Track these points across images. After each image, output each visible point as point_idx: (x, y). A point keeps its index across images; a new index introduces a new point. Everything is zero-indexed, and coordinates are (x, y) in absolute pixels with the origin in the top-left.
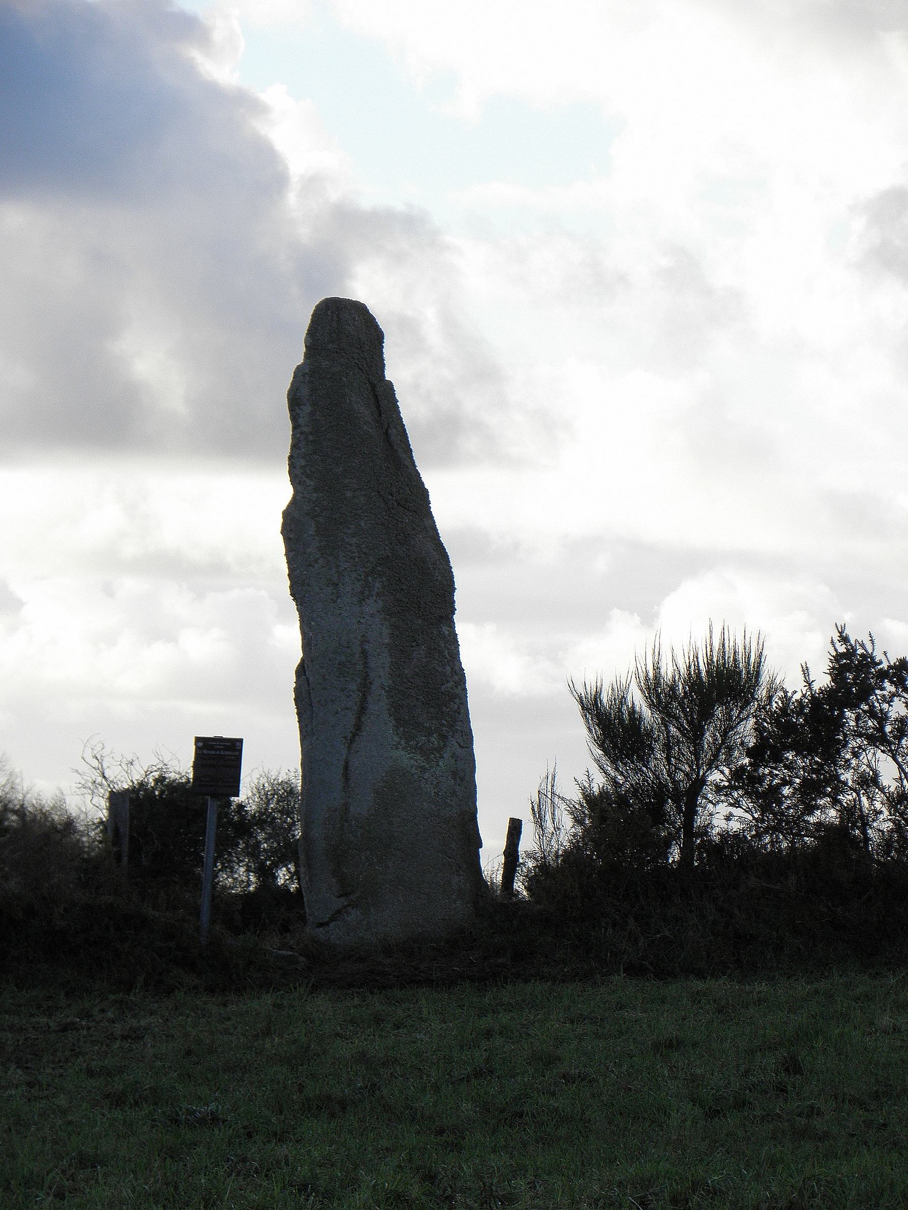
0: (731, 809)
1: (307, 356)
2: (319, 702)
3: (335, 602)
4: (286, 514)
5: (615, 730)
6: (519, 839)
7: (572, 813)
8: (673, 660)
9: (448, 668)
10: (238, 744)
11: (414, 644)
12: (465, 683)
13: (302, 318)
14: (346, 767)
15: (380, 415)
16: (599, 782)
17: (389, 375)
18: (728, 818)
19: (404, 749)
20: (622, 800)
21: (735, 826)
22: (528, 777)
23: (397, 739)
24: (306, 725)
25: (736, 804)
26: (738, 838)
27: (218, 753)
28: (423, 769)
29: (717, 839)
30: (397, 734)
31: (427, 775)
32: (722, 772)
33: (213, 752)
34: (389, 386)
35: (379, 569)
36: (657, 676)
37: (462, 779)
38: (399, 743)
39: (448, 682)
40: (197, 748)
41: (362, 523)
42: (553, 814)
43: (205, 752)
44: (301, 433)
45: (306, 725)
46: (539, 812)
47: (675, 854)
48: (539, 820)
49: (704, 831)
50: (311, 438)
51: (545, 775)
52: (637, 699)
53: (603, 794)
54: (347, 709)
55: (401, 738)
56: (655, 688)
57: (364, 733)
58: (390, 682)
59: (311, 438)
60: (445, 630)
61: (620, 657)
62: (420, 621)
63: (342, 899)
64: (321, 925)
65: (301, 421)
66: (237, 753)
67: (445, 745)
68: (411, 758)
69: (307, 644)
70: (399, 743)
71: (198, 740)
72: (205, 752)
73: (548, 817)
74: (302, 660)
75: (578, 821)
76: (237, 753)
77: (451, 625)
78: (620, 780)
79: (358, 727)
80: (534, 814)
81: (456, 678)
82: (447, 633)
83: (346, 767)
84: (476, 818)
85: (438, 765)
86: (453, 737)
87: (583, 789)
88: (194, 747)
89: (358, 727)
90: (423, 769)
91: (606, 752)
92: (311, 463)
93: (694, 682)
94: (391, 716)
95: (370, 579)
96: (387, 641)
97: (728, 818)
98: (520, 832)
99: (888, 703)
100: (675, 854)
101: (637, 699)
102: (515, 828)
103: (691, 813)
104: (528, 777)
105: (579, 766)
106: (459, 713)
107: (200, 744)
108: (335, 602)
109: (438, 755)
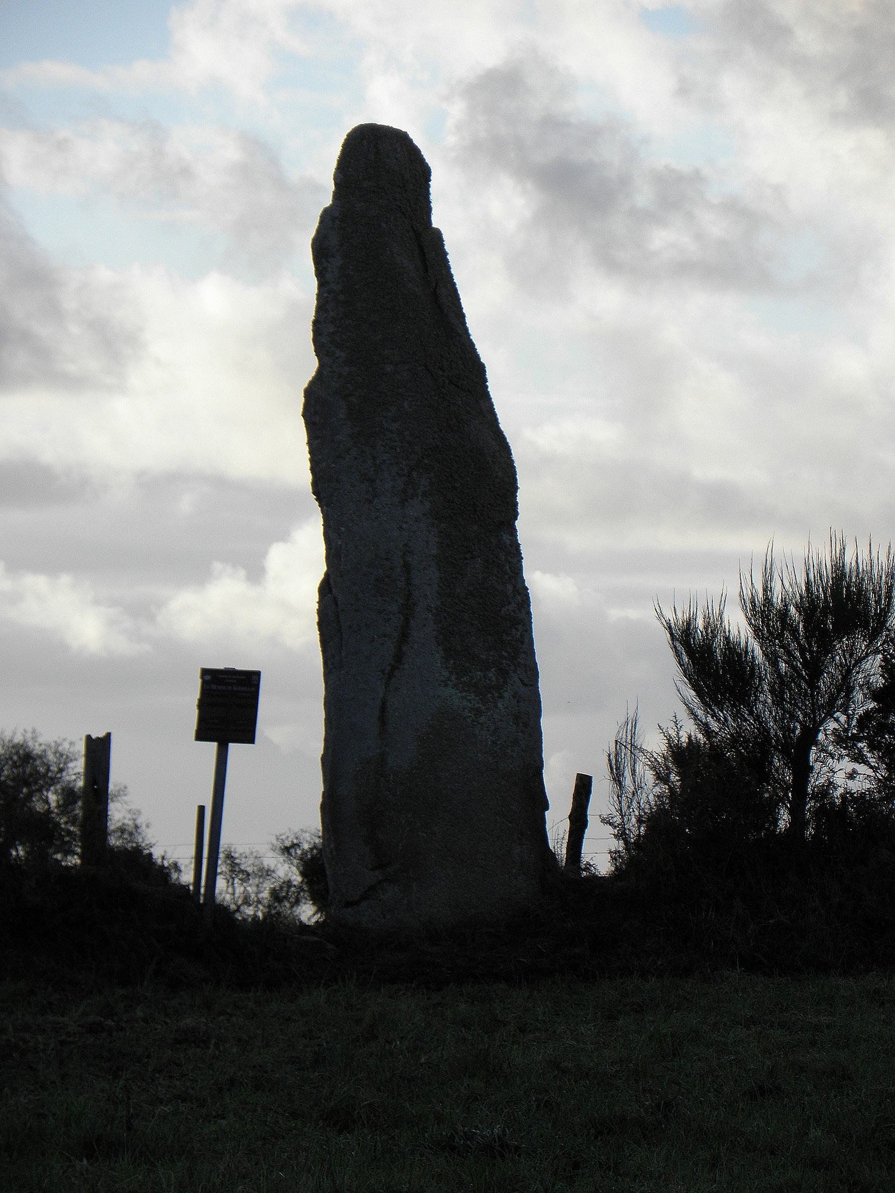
0: (857, 766)
1: (337, 195)
2: (350, 627)
3: (370, 502)
4: (309, 393)
5: (707, 662)
6: (588, 801)
7: (653, 768)
8: (857, 562)
9: (510, 587)
10: (254, 677)
11: (468, 556)
12: (529, 606)
13: (315, 175)
14: (383, 709)
15: (426, 270)
16: (689, 730)
17: (437, 221)
18: (852, 776)
19: (455, 686)
20: (715, 753)
21: (858, 786)
22: (604, 723)
23: (446, 673)
24: (333, 656)
25: (859, 758)
26: (860, 800)
27: (230, 688)
28: (478, 712)
29: (838, 802)
30: (447, 668)
31: (482, 719)
32: (837, 720)
33: (224, 688)
34: (437, 236)
35: (426, 461)
36: (768, 601)
37: (526, 725)
38: (449, 679)
39: (510, 603)
40: (204, 683)
41: (406, 405)
42: (634, 772)
43: (214, 687)
44: (329, 292)
45: (333, 656)
46: (618, 769)
47: (784, 819)
48: (617, 778)
49: (824, 792)
50: (342, 297)
51: (623, 720)
52: (738, 625)
53: (692, 743)
54: (385, 636)
55: (451, 673)
56: (766, 615)
57: (406, 666)
58: (439, 603)
59: (342, 297)
60: (506, 537)
61: (725, 574)
62: (476, 528)
63: (377, 873)
64: (349, 904)
65: (329, 276)
66: (253, 689)
67: (505, 683)
68: (463, 698)
69: (333, 555)
70: (449, 679)
71: (205, 672)
72: (214, 687)
73: (627, 773)
74: (327, 575)
75: (662, 778)
76: (253, 689)
77: (513, 532)
78: (714, 726)
79: (399, 657)
80: (611, 768)
81: (519, 599)
82: (508, 542)
83: (383, 709)
84: (541, 774)
85: (496, 707)
86: (515, 672)
87: (669, 739)
88: (200, 681)
89: (399, 657)
90: (478, 712)
91: (699, 693)
92: (338, 325)
93: (810, 606)
94: (439, 645)
95: (414, 474)
96: (434, 552)
97: (852, 776)
98: (589, 792)
99: (11, 759)
100: (784, 819)
101: (738, 625)
102: (583, 785)
103: (803, 770)
104: (604, 723)
105: (666, 712)
106: (522, 643)
107: (208, 678)
108: (370, 502)
109: (496, 695)
